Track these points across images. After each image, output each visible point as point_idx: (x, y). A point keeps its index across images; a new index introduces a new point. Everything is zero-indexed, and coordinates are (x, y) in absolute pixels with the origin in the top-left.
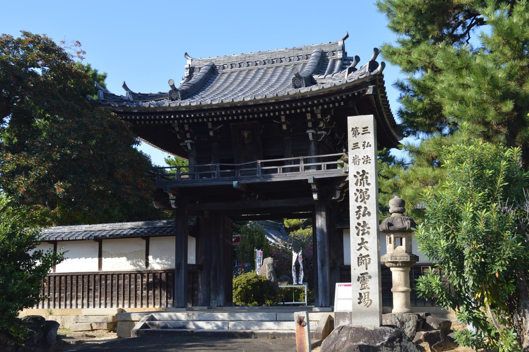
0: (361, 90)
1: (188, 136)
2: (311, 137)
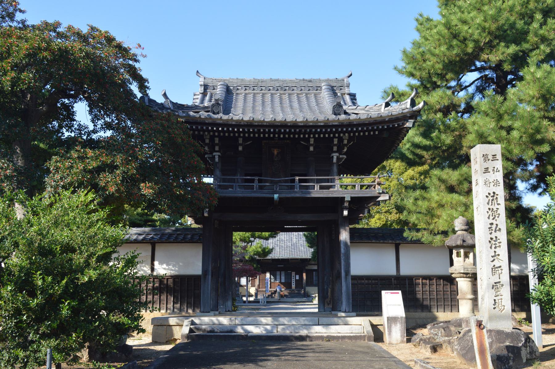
0: (401, 123)
1: (217, 148)
2: (335, 160)
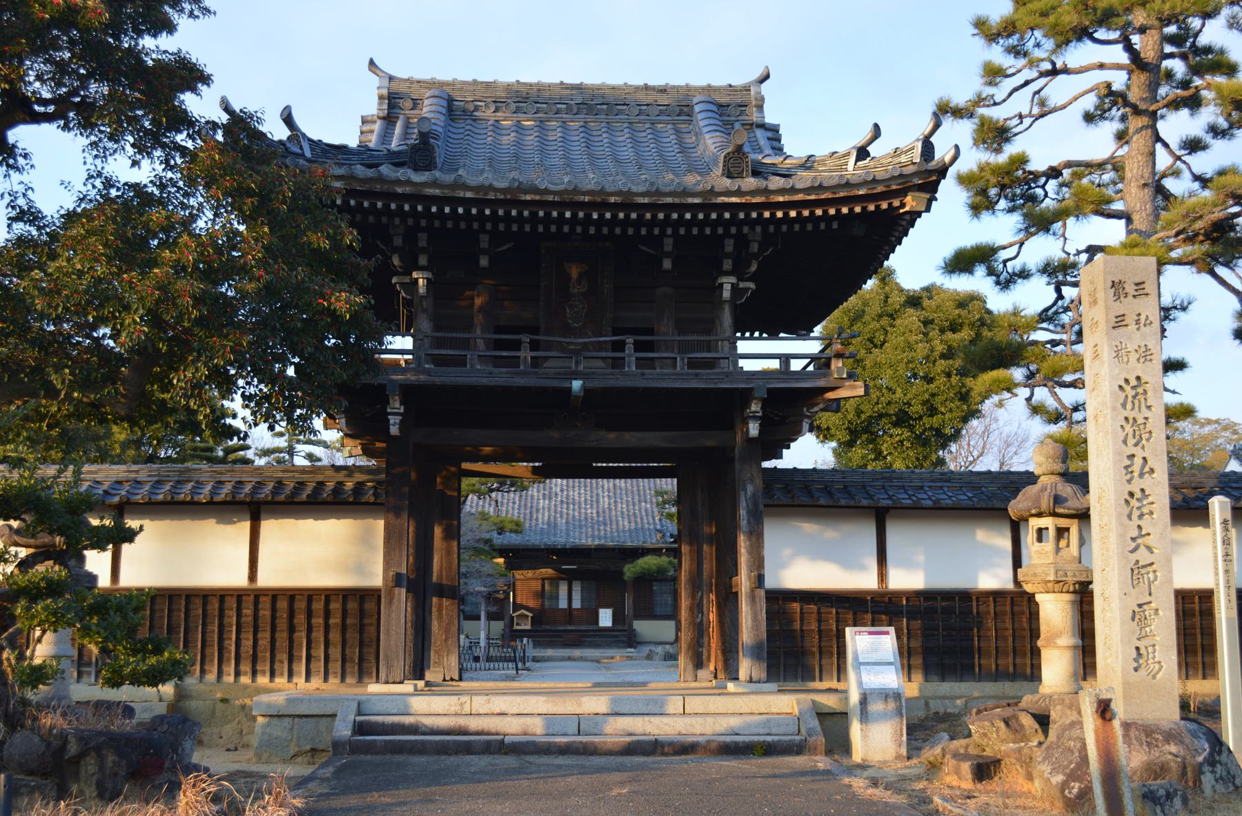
1: (423, 260)
2: (726, 294)
